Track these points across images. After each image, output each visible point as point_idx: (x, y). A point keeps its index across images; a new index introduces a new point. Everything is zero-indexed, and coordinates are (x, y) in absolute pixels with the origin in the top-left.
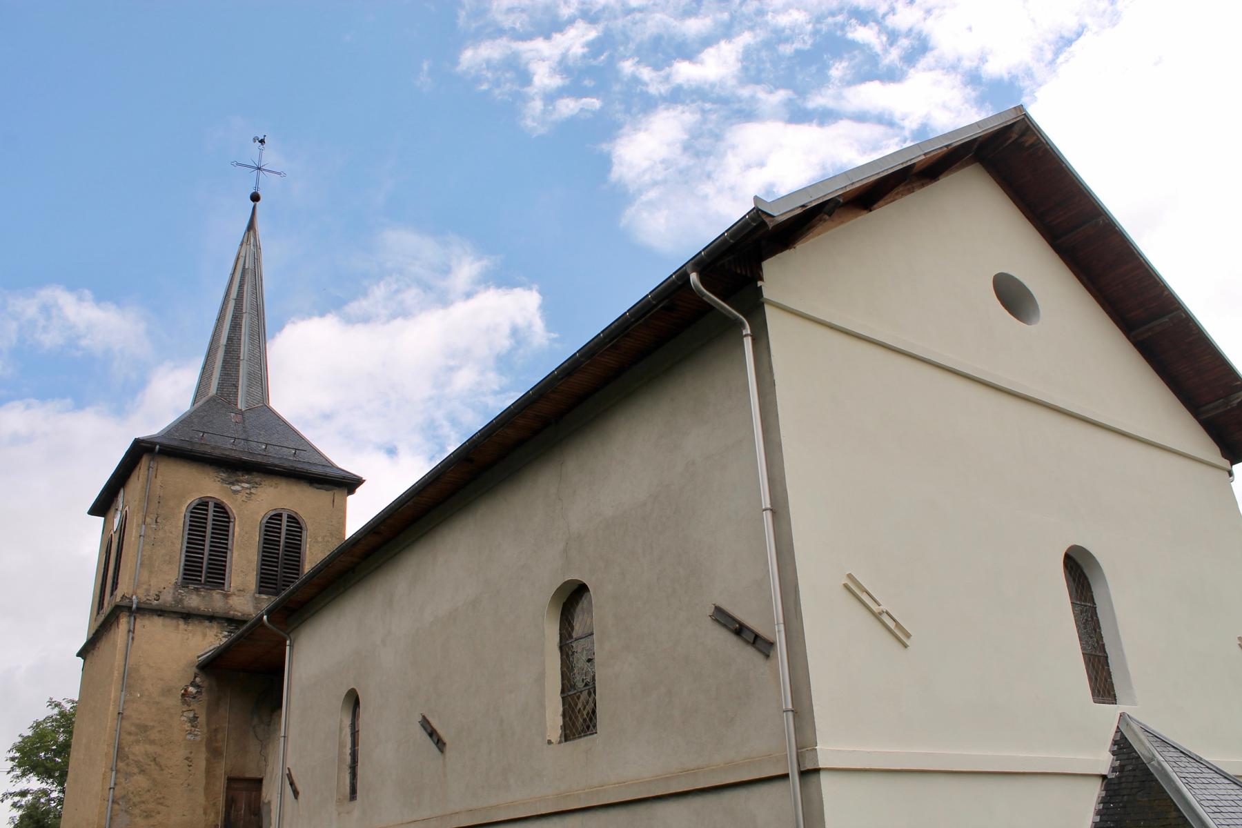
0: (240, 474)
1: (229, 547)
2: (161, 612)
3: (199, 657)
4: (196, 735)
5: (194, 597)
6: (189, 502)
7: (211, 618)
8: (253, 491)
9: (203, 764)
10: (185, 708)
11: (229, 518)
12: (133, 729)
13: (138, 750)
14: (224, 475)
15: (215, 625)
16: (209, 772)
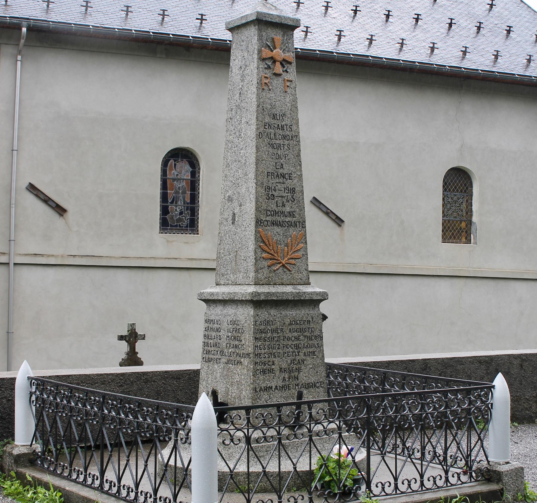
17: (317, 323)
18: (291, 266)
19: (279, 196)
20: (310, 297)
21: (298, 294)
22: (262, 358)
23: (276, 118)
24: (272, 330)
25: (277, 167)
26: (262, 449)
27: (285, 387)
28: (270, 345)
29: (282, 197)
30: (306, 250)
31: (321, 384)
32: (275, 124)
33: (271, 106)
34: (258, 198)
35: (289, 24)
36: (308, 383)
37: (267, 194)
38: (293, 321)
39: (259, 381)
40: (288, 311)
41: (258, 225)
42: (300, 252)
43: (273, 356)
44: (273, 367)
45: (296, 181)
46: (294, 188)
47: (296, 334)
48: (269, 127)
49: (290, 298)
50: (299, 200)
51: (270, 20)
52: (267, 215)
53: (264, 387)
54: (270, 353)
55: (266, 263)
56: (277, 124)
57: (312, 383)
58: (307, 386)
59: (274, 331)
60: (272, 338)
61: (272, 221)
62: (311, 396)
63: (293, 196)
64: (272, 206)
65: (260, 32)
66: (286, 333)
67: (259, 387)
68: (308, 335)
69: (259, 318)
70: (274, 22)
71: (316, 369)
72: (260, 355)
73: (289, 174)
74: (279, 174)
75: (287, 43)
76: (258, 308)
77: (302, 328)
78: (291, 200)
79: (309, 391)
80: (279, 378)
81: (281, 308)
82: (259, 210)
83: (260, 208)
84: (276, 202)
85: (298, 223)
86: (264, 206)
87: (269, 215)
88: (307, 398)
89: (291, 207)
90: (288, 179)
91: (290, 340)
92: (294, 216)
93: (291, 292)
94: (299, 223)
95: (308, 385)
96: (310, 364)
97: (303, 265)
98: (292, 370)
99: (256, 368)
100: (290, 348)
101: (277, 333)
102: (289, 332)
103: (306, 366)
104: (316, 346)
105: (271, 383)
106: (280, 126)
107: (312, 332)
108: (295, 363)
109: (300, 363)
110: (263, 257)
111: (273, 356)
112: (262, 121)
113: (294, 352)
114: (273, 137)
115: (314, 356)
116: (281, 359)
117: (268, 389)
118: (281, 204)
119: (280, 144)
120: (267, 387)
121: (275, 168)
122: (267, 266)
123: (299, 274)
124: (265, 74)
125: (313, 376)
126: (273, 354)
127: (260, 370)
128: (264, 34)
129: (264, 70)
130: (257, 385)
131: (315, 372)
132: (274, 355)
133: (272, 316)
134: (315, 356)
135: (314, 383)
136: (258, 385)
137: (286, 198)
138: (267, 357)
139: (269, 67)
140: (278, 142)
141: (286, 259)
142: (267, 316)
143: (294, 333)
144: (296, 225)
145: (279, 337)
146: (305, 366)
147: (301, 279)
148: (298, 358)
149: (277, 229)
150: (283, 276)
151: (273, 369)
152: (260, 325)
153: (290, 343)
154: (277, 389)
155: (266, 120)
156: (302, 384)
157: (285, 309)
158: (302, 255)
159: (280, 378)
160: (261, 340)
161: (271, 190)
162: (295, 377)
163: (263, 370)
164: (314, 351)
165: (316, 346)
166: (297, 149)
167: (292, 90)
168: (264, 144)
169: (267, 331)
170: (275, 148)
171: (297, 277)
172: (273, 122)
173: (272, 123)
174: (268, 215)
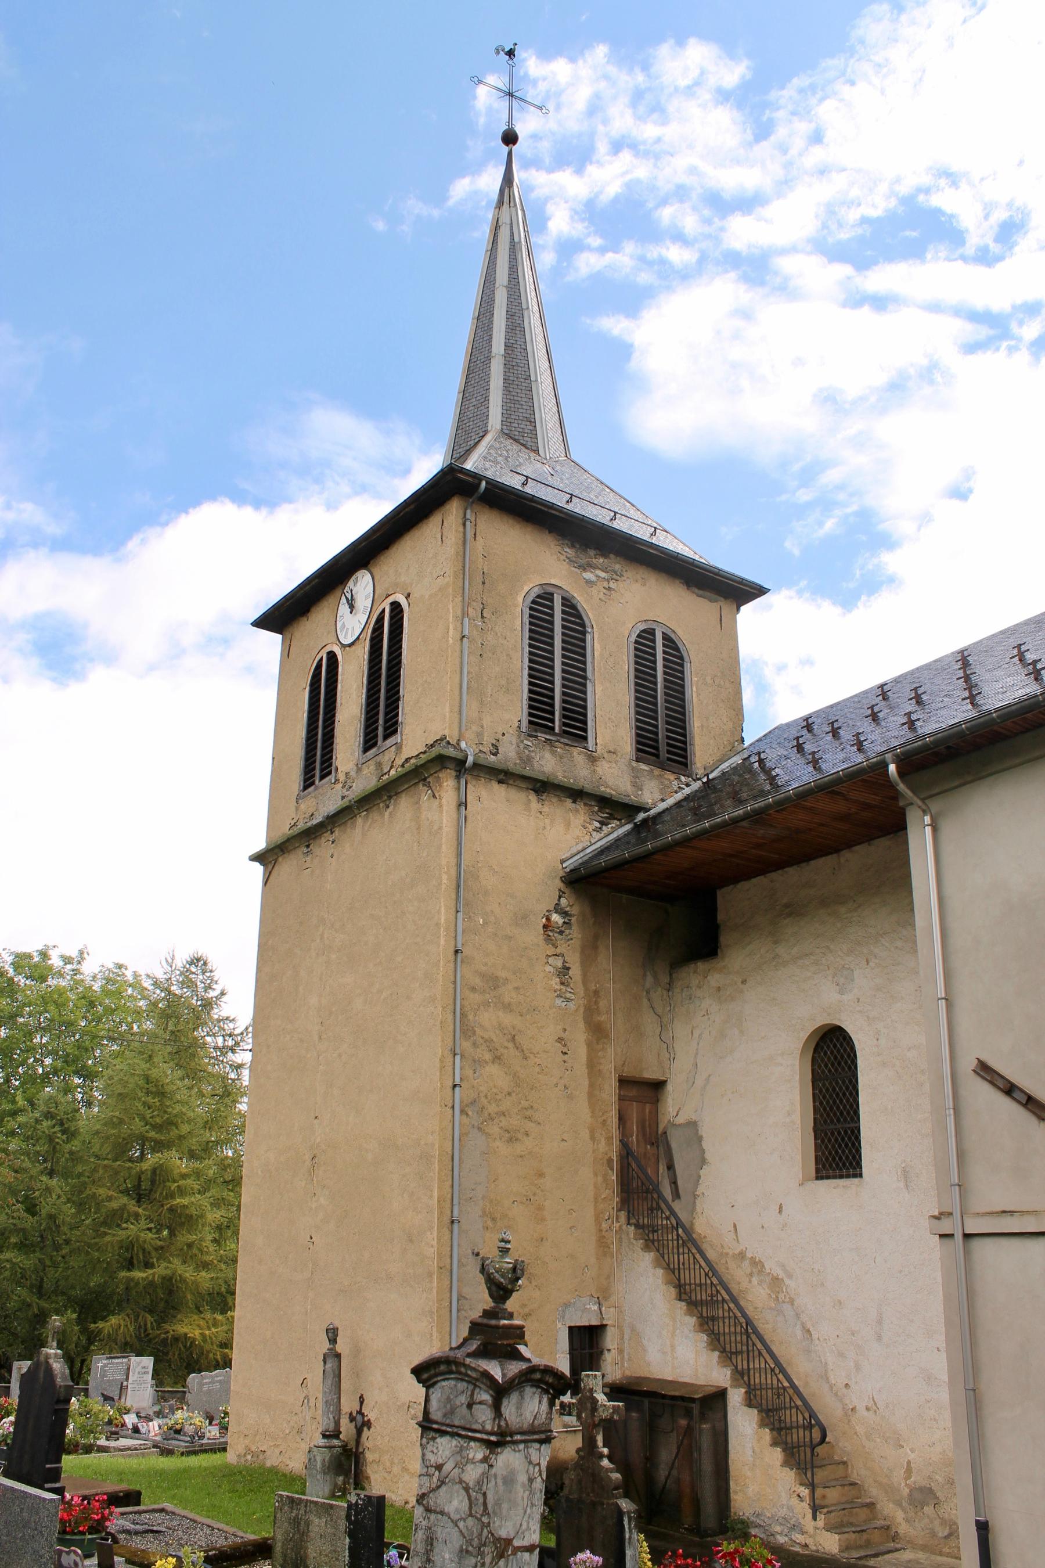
0: (592, 552)
1: (589, 674)
2: (503, 776)
3: (562, 862)
4: (568, 1000)
5: (547, 755)
6: (526, 589)
7: (576, 794)
8: (612, 585)
9: (582, 1052)
10: (551, 950)
11: (583, 625)
12: (477, 981)
13: (488, 1019)
14: (570, 552)
15: (580, 806)
16: (592, 1065)
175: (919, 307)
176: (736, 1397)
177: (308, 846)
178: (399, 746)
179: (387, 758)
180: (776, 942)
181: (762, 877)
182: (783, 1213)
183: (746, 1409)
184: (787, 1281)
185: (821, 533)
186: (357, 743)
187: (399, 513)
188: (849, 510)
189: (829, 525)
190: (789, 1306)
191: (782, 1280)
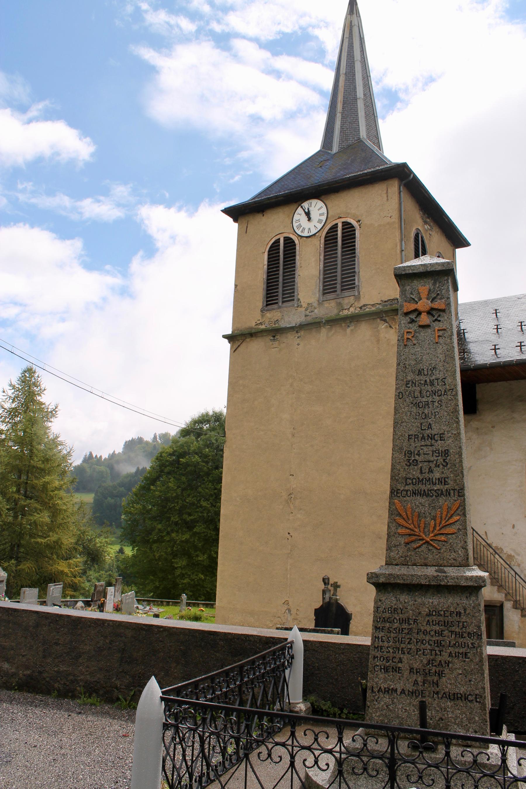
17: (473, 616)
18: (440, 543)
19: (425, 461)
20: (455, 582)
21: (436, 578)
22: (383, 652)
23: (422, 374)
24: (401, 619)
25: (423, 428)
26: (356, 765)
27: (417, 692)
28: (396, 637)
29: (429, 461)
30: (463, 524)
31: (476, 698)
32: (421, 380)
33: (416, 361)
34: (394, 465)
35: (438, 269)
36: (454, 693)
37: (407, 459)
38: (433, 611)
39: (377, 679)
40: (427, 598)
41: (393, 496)
42: (454, 527)
43: (400, 652)
44: (400, 665)
45: (450, 441)
46: (447, 450)
47: (437, 628)
48: (412, 385)
49: (423, 582)
50: (454, 464)
51: (411, 272)
52: (406, 483)
53: (385, 688)
54: (396, 648)
55: (402, 540)
56: (424, 379)
57: (460, 694)
58: (452, 697)
59: (404, 621)
60: (401, 629)
61: (413, 490)
62: (459, 712)
63: (446, 459)
64: (414, 473)
65: (403, 288)
66: (422, 625)
67: (377, 687)
68: (457, 630)
69: (382, 603)
70: (416, 273)
71: (469, 677)
72: (381, 649)
73: (441, 434)
74: (425, 435)
75: (439, 291)
76: (383, 591)
77: (448, 621)
78: (443, 465)
79: (455, 704)
80: (408, 680)
81: (417, 594)
82: (395, 479)
83: (397, 476)
84: (420, 468)
85: (452, 492)
86: (403, 474)
87: (410, 484)
88: (452, 712)
89: (443, 473)
90: (438, 440)
91: (428, 634)
92: (446, 483)
93: (425, 575)
94: (454, 492)
95: (454, 696)
96: (459, 669)
97: (459, 542)
98: (429, 673)
99: (375, 663)
100: (427, 645)
101: (408, 623)
102: (427, 624)
103: (452, 670)
104: (470, 645)
105: (396, 684)
106: (428, 381)
107: (463, 627)
108: (434, 665)
109: (442, 665)
110: (398, 533)
111: (400, 652)
112: (403, 380)
113: (434, 650)
114: (418, 395)
115: (466, 658)
116: (413, 656)
117: (390, 691)
118: (427, 470)
119: (428, 402)
120: (389, 689)
121: (420, 429)
122: (404, 543)
123: (451, 553)
124: (409, 329)
125: (462, 685)
126: (400, 649)
127: (381, 666)
128: (408, 288)
129: (407, 325)
130: (375, 683)
131: (467, 680)
132: (402, 651)
133: (401, 603)
134: (467, 660)
135: (465, 694)
136: (376, 684)
137: (435, 462)
138: (391, 652)
139: (412, 321)
140: (424, 399)
141: (432, 535)
142: (394, 602)
143: (435, 627)
144: (449, 494)
145: (411, 629)
146: (450, 671)
147: (454, 559)
148: (439, 658)
149: (420, 500)
150: (427, 556)
151: (399, 668)
152: (383, 612)
153: (427, 638)
154: (404, 693)
155: (408, 377)
156: (444, 693)
157: (422, 596)
158: (458, 530)
159: (410, 680)
160: (383, 631)
161: (413, 455)
162: (433, 682)
163: (384, 667)
164: (466, 653)
165: (470, 645)
166: (453, 404)
167: (446, 339)
168: (405, 404)
169: (394, 620)
170: (421, 406)
171: (448, 557)
172: (417, 378)
173: (417, 380)
174: (408, 483)
175: (297, 81)
176: (508, 606)
177: (274, 337)
178: (358, 298)
179: (346, 302)
180: (513, 412)
181: (505, 382)
182: (515, 528)
183: (514, 610)
184: (516, 557)
185: (232, 181)
186: (318, 290)
187: (358, 178)
188: (248, 173)
189: (237, 178)
190: (518, 567)
191: (514, 556)
